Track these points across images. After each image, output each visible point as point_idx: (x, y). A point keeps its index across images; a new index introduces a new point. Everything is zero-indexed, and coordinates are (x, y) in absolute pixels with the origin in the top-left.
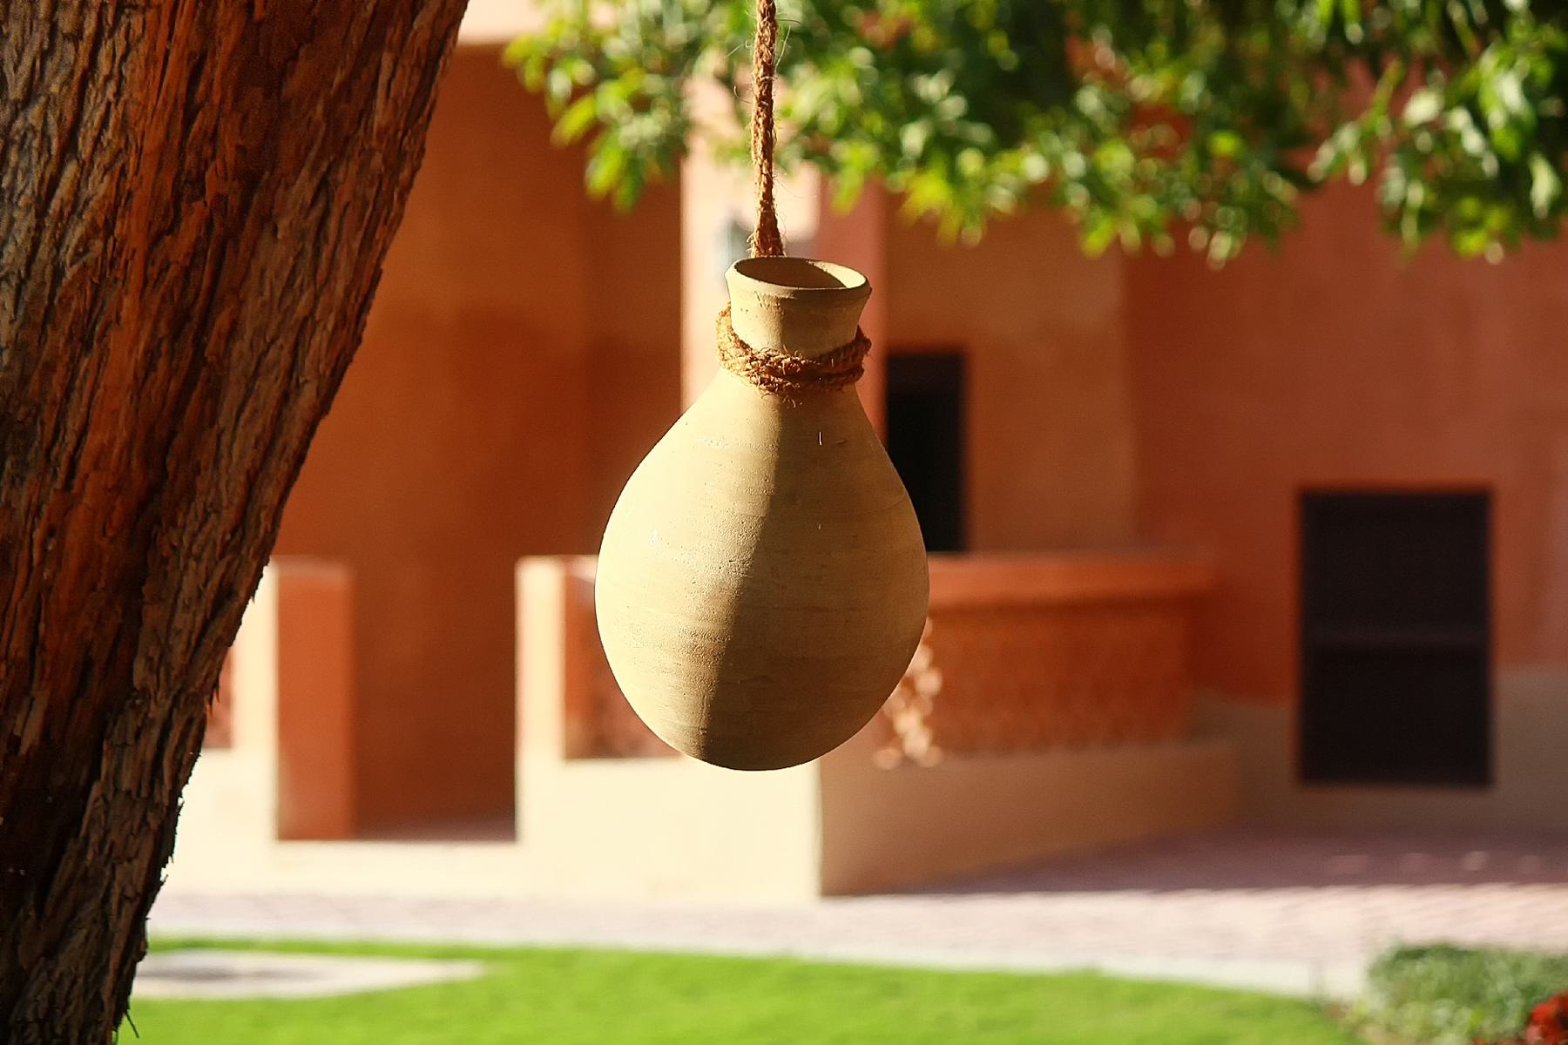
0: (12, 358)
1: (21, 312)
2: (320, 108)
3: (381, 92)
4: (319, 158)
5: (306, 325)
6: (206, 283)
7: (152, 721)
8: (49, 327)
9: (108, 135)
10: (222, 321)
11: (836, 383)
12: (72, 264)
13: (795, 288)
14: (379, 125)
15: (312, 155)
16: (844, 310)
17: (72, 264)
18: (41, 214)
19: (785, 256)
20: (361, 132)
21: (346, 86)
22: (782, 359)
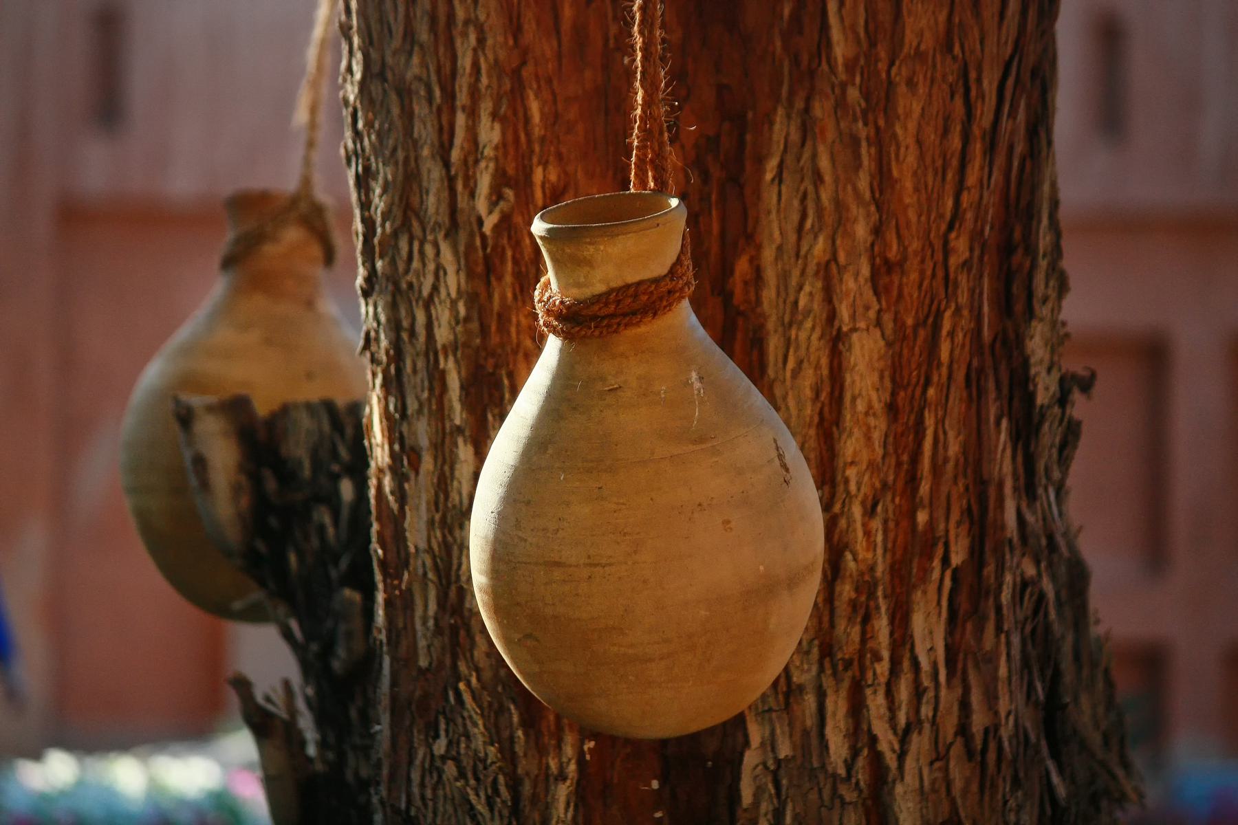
0: (468, 309)
1: (463, 262)
2: (778, 44)
3: (833, 20)
4: (792, 93)
5: (828, 273)
6: (716, 227)
7: (801, 688)
8: (493, 279)
9: (484, 80)
10: (742, 266)
11: (608, 326)
12: (490, 212)
13: (560, 226)
14: (843, 56)
15: (785, 90)
16: (602, 248)
17: (490, 212)
18: (447, 164)
19: (632, 191)
20: (825, 66)
21: (796, 17)
22: (634, 302)
